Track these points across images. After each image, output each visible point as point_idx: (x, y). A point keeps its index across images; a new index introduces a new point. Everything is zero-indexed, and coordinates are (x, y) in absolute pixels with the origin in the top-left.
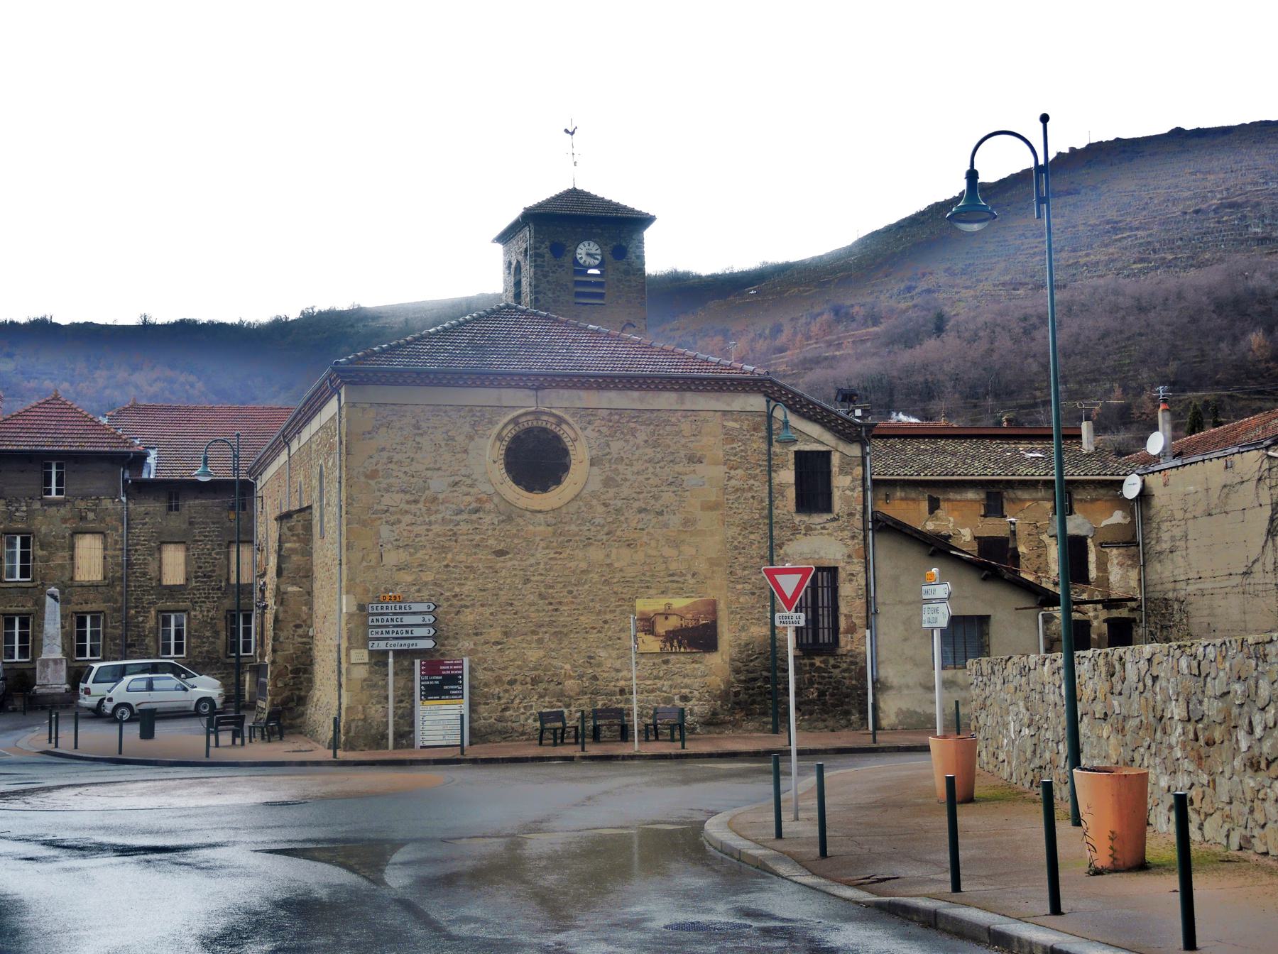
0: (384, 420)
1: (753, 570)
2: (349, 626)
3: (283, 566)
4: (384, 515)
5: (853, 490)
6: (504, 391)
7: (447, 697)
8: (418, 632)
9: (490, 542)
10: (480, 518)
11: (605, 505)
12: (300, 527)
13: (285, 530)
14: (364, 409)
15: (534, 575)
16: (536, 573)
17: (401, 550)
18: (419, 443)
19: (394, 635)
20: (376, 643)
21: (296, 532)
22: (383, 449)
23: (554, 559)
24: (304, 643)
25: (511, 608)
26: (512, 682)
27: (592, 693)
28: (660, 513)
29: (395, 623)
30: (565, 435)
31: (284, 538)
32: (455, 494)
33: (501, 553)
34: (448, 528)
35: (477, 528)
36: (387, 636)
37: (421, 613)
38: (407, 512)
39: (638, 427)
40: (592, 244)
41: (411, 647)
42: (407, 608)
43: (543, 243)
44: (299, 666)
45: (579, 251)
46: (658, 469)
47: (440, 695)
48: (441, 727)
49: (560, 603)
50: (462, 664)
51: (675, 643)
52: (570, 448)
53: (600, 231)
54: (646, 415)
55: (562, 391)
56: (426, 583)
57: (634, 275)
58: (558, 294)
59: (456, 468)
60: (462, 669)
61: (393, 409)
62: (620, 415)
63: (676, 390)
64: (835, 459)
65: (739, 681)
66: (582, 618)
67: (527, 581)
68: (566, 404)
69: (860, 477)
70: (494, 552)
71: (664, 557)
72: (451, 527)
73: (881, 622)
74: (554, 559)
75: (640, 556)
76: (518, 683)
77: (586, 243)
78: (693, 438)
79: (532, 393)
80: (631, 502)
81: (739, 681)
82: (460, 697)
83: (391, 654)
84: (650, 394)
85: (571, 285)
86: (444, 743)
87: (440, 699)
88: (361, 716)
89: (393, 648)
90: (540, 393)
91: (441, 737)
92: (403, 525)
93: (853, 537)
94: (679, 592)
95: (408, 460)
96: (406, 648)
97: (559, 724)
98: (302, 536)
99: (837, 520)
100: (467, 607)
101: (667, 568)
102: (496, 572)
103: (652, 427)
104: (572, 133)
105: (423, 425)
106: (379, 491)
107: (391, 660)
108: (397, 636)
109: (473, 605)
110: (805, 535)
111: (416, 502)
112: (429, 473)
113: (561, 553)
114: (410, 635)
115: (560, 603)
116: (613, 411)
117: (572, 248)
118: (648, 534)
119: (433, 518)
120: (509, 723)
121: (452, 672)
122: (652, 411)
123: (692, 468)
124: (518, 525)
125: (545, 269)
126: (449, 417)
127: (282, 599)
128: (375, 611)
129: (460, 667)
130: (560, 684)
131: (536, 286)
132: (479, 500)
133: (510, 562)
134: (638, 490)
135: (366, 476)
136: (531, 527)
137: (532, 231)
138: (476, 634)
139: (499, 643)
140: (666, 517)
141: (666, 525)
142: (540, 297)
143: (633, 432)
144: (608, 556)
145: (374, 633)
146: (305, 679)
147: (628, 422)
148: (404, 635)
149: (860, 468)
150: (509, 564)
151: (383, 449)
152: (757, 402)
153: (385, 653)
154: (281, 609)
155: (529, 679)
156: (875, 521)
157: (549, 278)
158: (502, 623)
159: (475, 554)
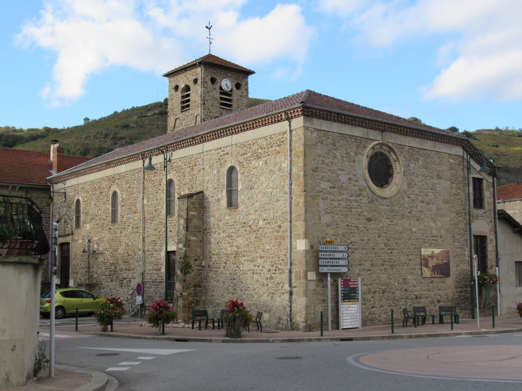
0: (320, 139)
1: (460, 235)
2: (307, 258)
3: (189, 225)
4: (320, 194)
5: (490, 199)
6: (369, 130)
7: (352, 300)
8: (342, 262)
9: (365, 213)
10: (361, 200)
11: (409, 197)
12: (197, 203)
13: (190, 204)
14: (312, 131)
15: (382, 233)
16: (383, 232)
17: (328, 215)
18: (335, 154)
19: (331, 264)
20: (323, 268)
21: (195, 206)
22: (320, 156)
23: (390, 225)
24: (199, 270)
25: (374, 251)
26: (374, 292)
27: (405, 299)
28: (428, 204)
29: (331, 257)
30: (392, 158)
31: (189, 209)
32: (350, 185)
33: (369, 220)
34: (347, 204)
35: (359, 205)
36: (328, 264)
37: (341, 252)
38: (330, 193)
39: (420, 157)
40: (228, 80)
41: (338, 271)
42: (336, 248)
43: (208, 76)
44: (196, 283)
45: (222, 83)
46: (427, 180)
47: (349, 299)
48: (350, 318)
49: (393, 249)
50: (358, 282)
51: (436, 273)
52: (393, 165)
53: (231, 75)
54: (422, 152)
55: (391, 134)
56: (339, 234)
57: (244, 98)
58: (213, 102)
59: (351, 171)
60: (358, 285)
61: (324, 133)
62: (413, 150)
63: (433, 140)
64: (485, 182)
65: (457, 292)
66: (401, 257)
67: (380, 236)
68: (393, 142)
69: (492, 193)
70: (366, 219)
71: (430, 227)
72: (349, 203)
73: (501, 263)
74: (390, 225)
75: (422, 226)
76: (377, 293)
77: (225, 79)
78: (438, 166)
79: (380, 133)
80: (418, 196)
81: (457, 292)
82: (357, 300)
83: (329, 275)
84: (424, 141)
85: (219, 99)
86: (351, 327)
87: (349, 301)
88: (312, 311)
89: (331, 271)
90: (384, 134)
91: (350, 323)
92: (329, 201)
93: (491, 222)
94: (436, 246)
95: (331, 163)
96: (336, 271)
97: (423, 314)
98: (197, 208)
99: (486, 213)
100: (356, 249)
101: (432, 233)
102: (368, 230)
103: (424, 158)
104: (210, 29)
105: (337, 145)
106: (319, 179)
107: (329, 278)
108: (332, 264)
109: (358, 248)
110: (477, 219)
111: (334, 188)
112: (339, 172)
113: (392, 222)
114: (338, 264)
115: (393, 249)
116: (412, 148)
117: (219, 81)
118: (424, 214)
119: (341, 197)
120: (374, 315)
121: (354, 286)
122: (424, 150)
123: (439, 181)
124: (376, 205)
125: (208, 89)
126: (347, 141)
127: (189, 244)
128: (323, 250)
129: (357, 283)
130: (393, 293)
131: (204, 97)
132: (360, 190)
133: (372, 225)
134: (420, 191)
135: (313, 170)
136: (381, 206)
137: (203, 70)
138: (360, 265)
139: (369, 270)
140: (431, 206)
141: (430, 210)
142: (206, 102)
143: (418, 159)
144: (410, 224)
145: (322, 262)
146: (199, 290)
147: (415, 154)
148: (336, 264)
149: (492, 188)
150: (373, 226)
151: (320, 156)
152: (459, 151)
153: (326, 274)
154: (188, 249)
155: (381, 291)
156: (499, 214)
157: (210, 94)
158: (371, 259)
159: (359, 219)
